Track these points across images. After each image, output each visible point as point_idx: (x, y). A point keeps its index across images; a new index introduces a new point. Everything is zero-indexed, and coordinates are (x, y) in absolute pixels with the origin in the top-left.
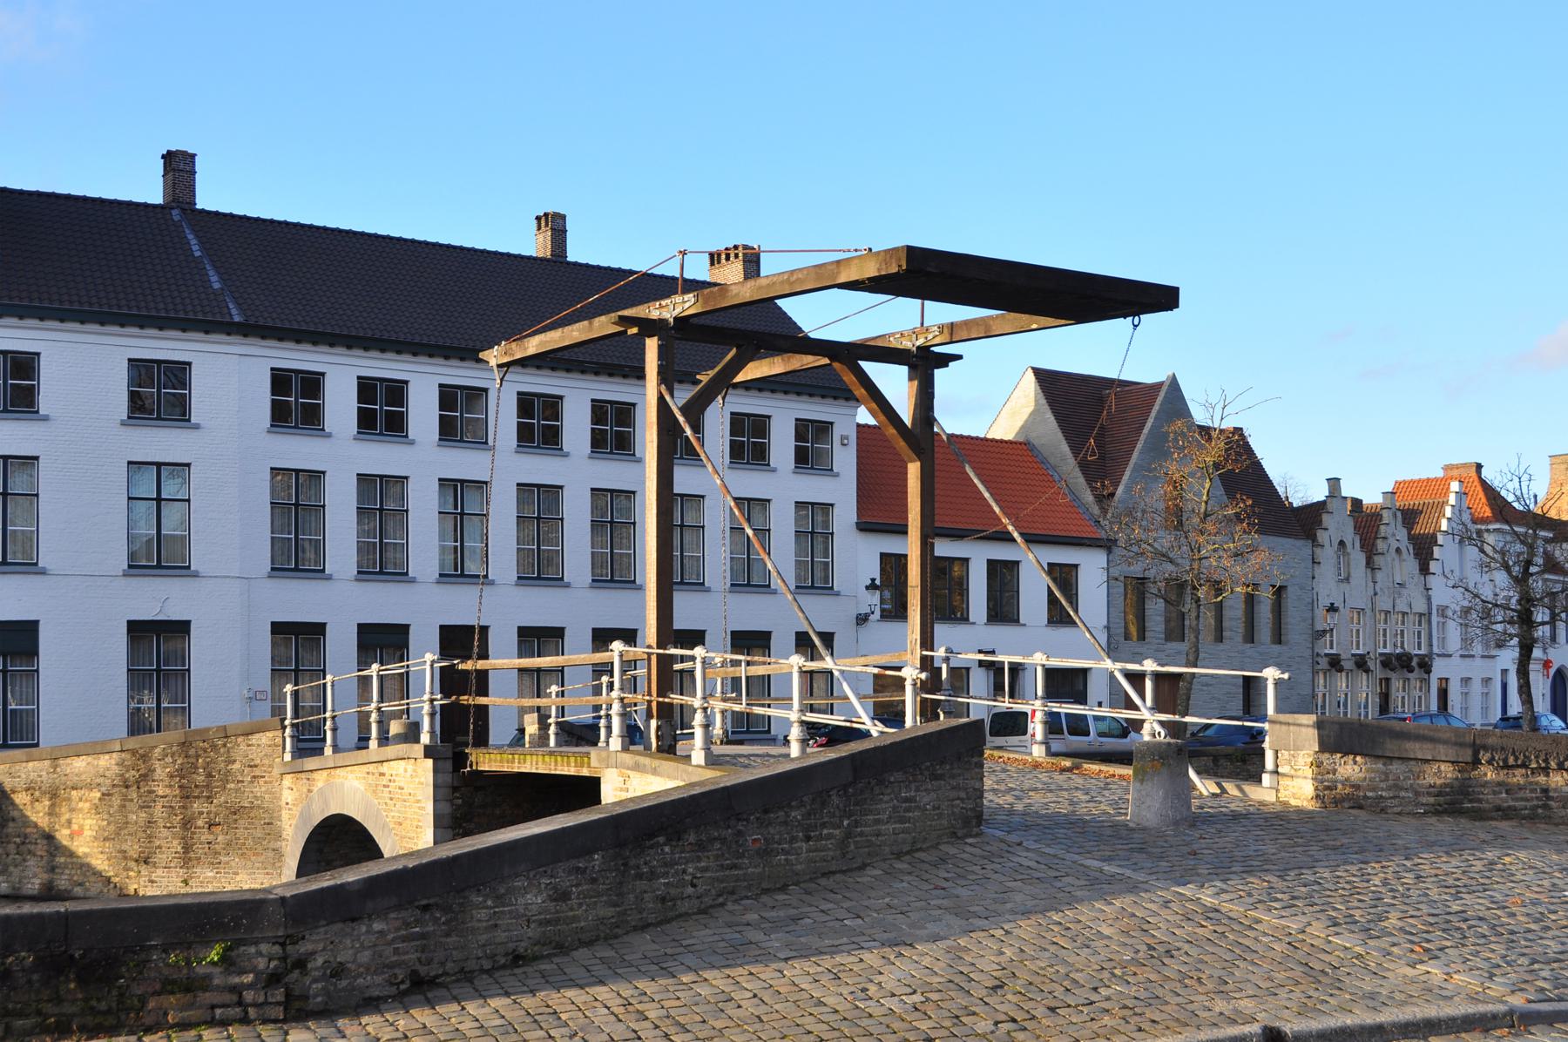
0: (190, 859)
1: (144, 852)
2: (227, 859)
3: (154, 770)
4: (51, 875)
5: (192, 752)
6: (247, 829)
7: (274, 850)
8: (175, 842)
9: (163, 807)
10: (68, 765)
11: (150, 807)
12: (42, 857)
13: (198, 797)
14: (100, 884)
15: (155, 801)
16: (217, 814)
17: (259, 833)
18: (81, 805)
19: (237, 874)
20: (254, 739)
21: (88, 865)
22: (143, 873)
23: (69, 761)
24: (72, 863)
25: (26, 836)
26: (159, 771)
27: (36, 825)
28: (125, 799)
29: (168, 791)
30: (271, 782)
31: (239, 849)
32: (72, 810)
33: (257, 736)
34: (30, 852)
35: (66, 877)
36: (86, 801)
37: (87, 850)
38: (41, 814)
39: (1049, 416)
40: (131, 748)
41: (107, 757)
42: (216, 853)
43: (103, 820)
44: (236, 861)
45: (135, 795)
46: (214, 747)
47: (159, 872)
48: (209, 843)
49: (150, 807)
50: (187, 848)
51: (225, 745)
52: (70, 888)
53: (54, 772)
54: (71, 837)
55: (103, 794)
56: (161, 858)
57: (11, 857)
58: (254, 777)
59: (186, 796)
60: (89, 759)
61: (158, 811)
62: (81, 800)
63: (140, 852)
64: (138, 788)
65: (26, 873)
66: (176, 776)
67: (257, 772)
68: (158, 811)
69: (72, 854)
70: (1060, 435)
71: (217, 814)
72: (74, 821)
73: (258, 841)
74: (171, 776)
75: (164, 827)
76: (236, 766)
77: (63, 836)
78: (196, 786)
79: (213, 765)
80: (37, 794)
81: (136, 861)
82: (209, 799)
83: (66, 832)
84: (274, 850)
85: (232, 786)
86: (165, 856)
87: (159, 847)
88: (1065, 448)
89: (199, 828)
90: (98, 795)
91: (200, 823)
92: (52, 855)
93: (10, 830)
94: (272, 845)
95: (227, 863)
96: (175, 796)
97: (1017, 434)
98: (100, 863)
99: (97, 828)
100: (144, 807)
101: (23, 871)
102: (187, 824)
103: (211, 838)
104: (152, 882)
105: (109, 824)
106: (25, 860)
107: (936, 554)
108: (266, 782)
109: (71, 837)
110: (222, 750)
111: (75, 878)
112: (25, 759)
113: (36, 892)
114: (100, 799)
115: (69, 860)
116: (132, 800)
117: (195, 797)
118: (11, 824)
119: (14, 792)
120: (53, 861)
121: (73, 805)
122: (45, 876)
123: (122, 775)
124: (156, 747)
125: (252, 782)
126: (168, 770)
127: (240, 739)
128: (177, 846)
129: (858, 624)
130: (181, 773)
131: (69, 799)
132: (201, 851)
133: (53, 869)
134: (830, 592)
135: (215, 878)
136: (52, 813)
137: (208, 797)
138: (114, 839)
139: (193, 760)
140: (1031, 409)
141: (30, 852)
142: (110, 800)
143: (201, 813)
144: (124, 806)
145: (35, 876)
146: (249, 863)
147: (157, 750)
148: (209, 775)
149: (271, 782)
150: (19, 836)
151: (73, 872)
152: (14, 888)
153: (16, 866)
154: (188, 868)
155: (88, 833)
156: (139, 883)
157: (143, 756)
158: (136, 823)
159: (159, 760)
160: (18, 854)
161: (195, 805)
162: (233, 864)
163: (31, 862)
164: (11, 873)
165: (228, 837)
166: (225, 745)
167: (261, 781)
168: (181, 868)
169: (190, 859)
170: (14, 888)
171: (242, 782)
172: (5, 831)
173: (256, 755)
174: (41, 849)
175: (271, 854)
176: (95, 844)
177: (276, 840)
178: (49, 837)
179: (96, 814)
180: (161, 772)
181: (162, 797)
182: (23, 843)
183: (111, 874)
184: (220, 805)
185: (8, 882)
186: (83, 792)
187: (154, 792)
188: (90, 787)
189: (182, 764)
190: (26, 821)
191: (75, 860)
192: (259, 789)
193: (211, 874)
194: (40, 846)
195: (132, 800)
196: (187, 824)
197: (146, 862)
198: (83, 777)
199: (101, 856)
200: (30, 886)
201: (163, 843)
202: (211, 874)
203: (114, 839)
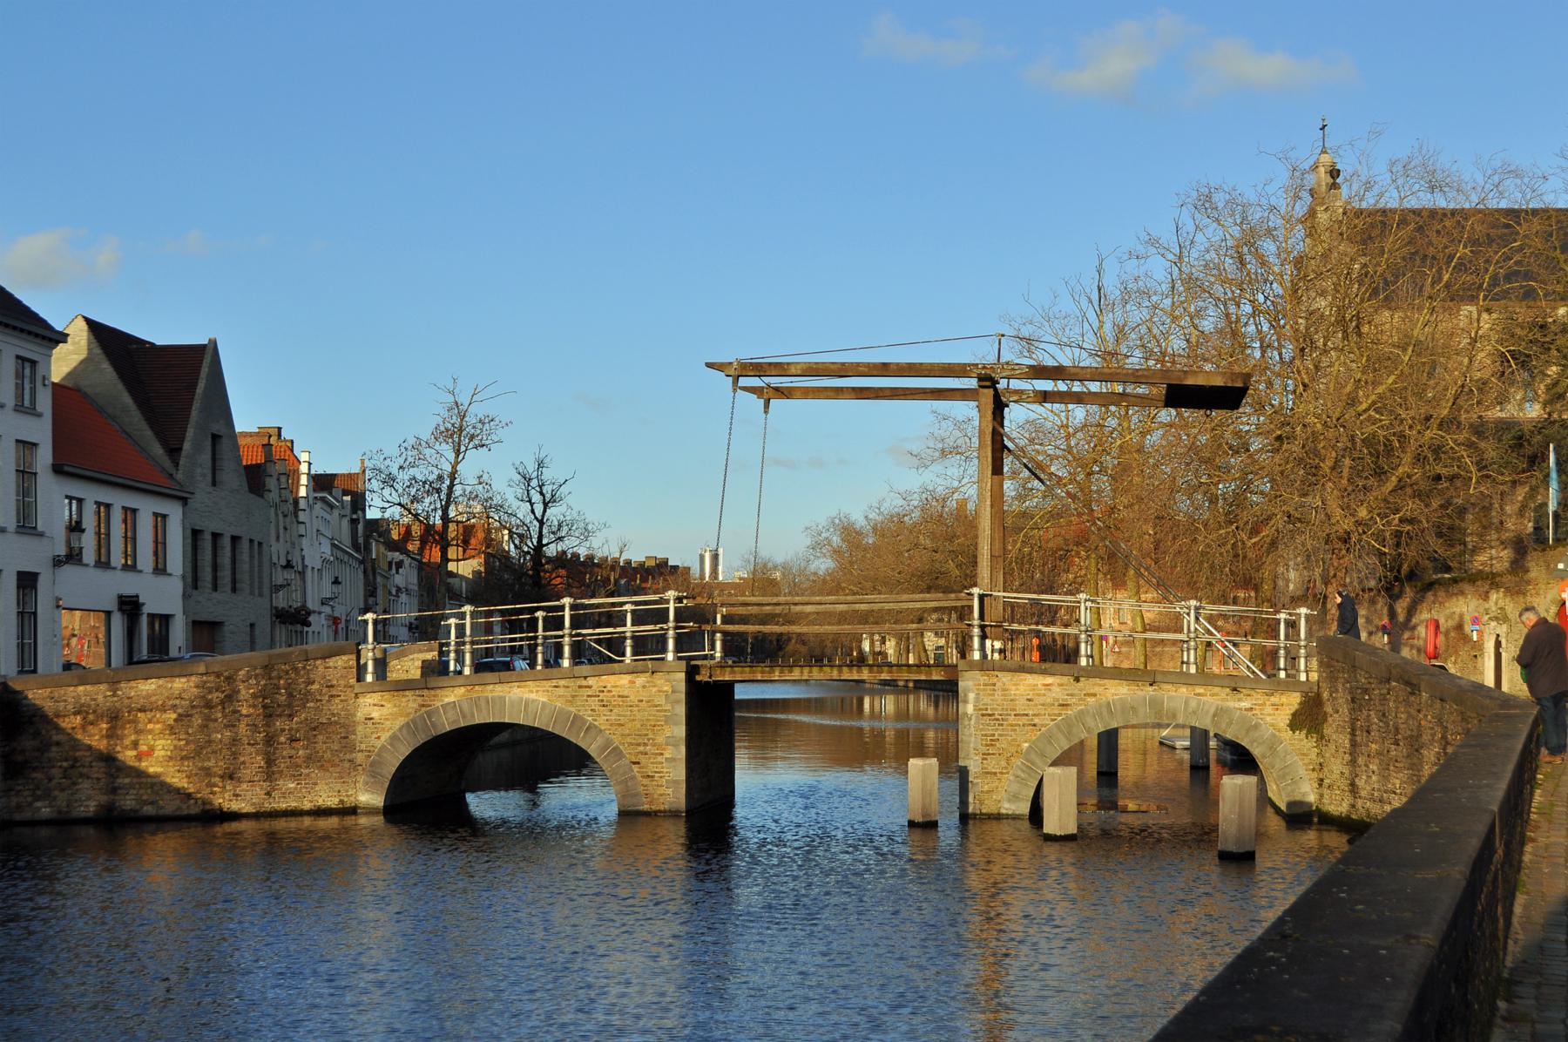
0: (273, 773)
1: (228, 768)
2: (307, 771)
3: (239, 691)
4: (112, 797)
5: (274, 674)
6: (325, 743)
7: (350, 761)
8: (259, 758)
9: (248, 725)
10: (131, 688)
11: (235, 726)
12: (98, 779)
13: (280, 716)
14: (178, 802)
15: (239, 720)
16: (297, 731)
17: (336, 747)
18: (150, 726)
19: (316, 784)
20: (331, 662)
21: (163, 784)
22: (228, 788)
23: (133, 684)
24: (140, 784)
25: (76, 760)
26: (243, 692)
27: (90, 748)
28: (208, 719)
29: (251, 710)
30: (346, 701)
31: (319, 761)
32: (138, 732)
33: (334, 659)
34: (82, 775)
35: (133, 797)
36: (158, 722)
37: (159, 770)
38: (97, 737)
39: (106, 366)
40: (216, 670)
41: (183, 680)
42: (297, 766)
43: (179, 740)
44: (315, 772)
45: (220, 715)
46: (296, 670)
47: (244, 786)
48: (290, 757)
49: (235, 726)
50: (270, 762)
51: (304, 668)
52: (138, 807)
53: (114, 696)
54: (139, 757)
55: (180, 715)
56: (246, 773)
57: (55, 781)
58: (332, 696)
59: (269, 715)
60: (161, 682)
61: (243, 728)
62: (150, 721)
63: (225, 769)
64: (224, 708)
65: (77, 796)
66: (260, 697)
67: (334, 692)
68: (243, 728)
69: (140, 774)
70: (120, 386)
71: (297, 731)
72: (141, 742)
73: (335, 753)
74: (254, 696)
75: (249, 744)
76: (316, 687)
77: (128, 756)
78: (279, 706)
79: (294, 686)
80: (91, 717)
81: (222, 777)
82: (291, 716)
83: (132, 753)
84: (350, 761)
85: (311, 704)
86: (249, 771)
87: (244, 763)
88: (127, 399)
89: (282, 743)
90: (174, 716)
91: (282, 739)
92: (113, 777)
93: (52, 755)
94: (347, 756)
95: (308, 775)
96: (259, 715)
97: (62, 379)
98: (177, 780)
99: (172, 748)
100: (228, 726)
101: (72, 794)
102: (270, 740)
103: (293, 752)
104: (237, 795)
105: (187, 744)
106: (75, 784)
107: (368, 517)
108: (342, 701)
109: (139, 757)
110: (302, 672)
111: (145, 797)
112: (75, 683)
113: (91, 814)
114: (176, 720)
115: (135, 780)
116: (216, 720)
117: (277, 716)
118: (54, 749)
119: (58, 716)
120: (113, 783)
121: (141, 726)
122: (104, 799)
123: (204, 697)
124: (240, 669)
125: (329, 701)
126: (251, 691)
127: (319, 662)
128: (260, 761)
129: (54, 566)
130: (263, 694)
131: (135, 721)
132: (282, 765)
133: (114, 791)
134: (34, 532)
135: (296, 788)
136: (111, 735)
137: (290, 715)
138: (193, 757)
139: (276, 681)
140: (82, 357)
141: (82, 775)
142: (189, 721)
143: (283, 730)
144: (206, 726)
145: (89, 798)
146: (327, 774)
147: (242, 673)
148: (290, 695)
149: (346, 701)
150: (66, 760)
151: (142, 792)
152: (60, 812)
153: (63, 790)
154: (271, 782)
155: (159, 753)
156: (224, 798)
157: (228, 678)
158: (221, 741)
159: (243, 682)
160: (65, 778)
161: (278, 723)
162: (313, 775)
163: (85, 785)
164: (55, 798)
165: (308, 751)
166: (304, 668)
167: (337, 700)
168: (264, 781)
169: (273, 773)
170: (60, 812)
171: (321, 700)
172: (46, 755)
173: (332, 676)
174: (98, 770)
175: (347, 765)
176: (171, 764)
177: (351, 752)
178: (109, 759)
179: (170, 735)
180: (245, 693)
181: (246, 716)
182: (73, 767)
183: (192, 790)
184: (301, 723)
185: (51, 806)
186: (153, 714)
187: (239, 711)
188: (163, 709)
189: (266, 685)
190: (75, 744)
191: (144, 780)
192: (336, 705)
193: (292, 785)
194: (95, 769)
195: (216, 720)
196: (270, 740)
197: (231, 777)
198: (154, 699)
199: (178, 775)
200: (82, 809)
201: (246, 759)
202: (292, 785)
203: (193, 757)
